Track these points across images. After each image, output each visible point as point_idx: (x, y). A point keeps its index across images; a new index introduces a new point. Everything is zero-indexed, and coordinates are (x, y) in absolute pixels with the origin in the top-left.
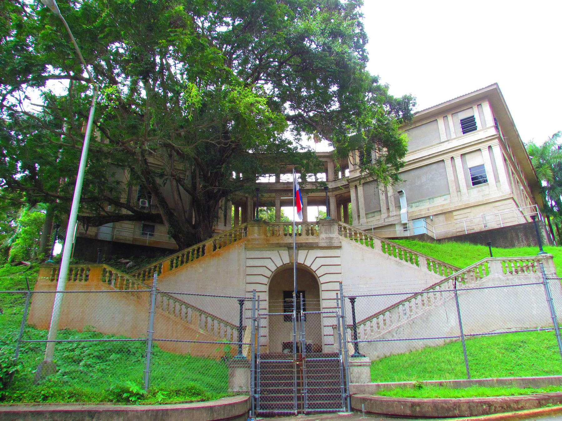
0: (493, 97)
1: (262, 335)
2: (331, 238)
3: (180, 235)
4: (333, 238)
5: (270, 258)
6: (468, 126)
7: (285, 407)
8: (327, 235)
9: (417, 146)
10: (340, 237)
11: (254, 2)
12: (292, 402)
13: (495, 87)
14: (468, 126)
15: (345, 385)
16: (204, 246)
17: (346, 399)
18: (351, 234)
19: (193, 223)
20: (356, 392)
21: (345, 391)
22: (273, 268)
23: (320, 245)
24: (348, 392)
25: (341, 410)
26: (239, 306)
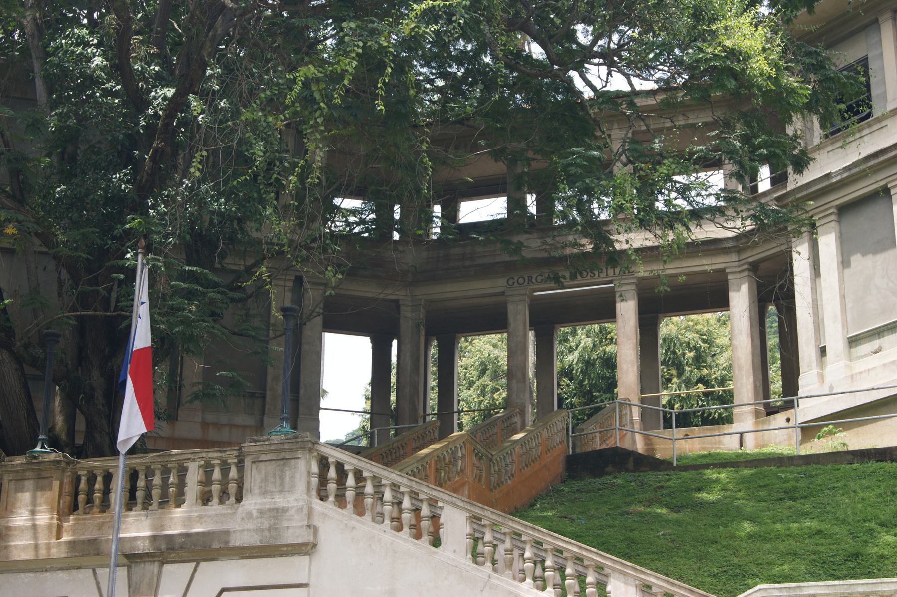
1: (738, 446)
2: (277, 513)
4: (284, 510)
5: (223, 590)
8: (267, 502)
10: (317, 504)
18: (360, 495)
19: (395, 343)
23: (237, 541)
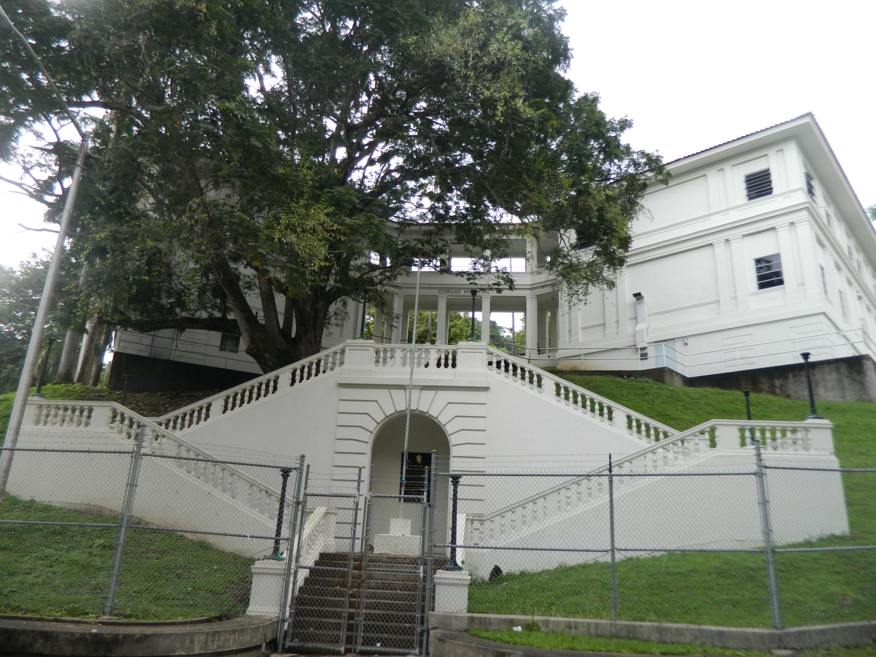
0: (805, 137)
3: (267, 355)
6: (759, 185)
7: (328, 641)
9: (655, 220)
11: (4, 89)
12: (338, 633)
13: (807, 120)
14: (759, 185)
15: (423, 611)
16: (277, 378)
17: (421, 634)
19: (293, 335)
20: (437, 626)
21: (422, 623)
22: (380, 417)
24: (425, 624)
25: (412, 651)
26: (281, 478)
